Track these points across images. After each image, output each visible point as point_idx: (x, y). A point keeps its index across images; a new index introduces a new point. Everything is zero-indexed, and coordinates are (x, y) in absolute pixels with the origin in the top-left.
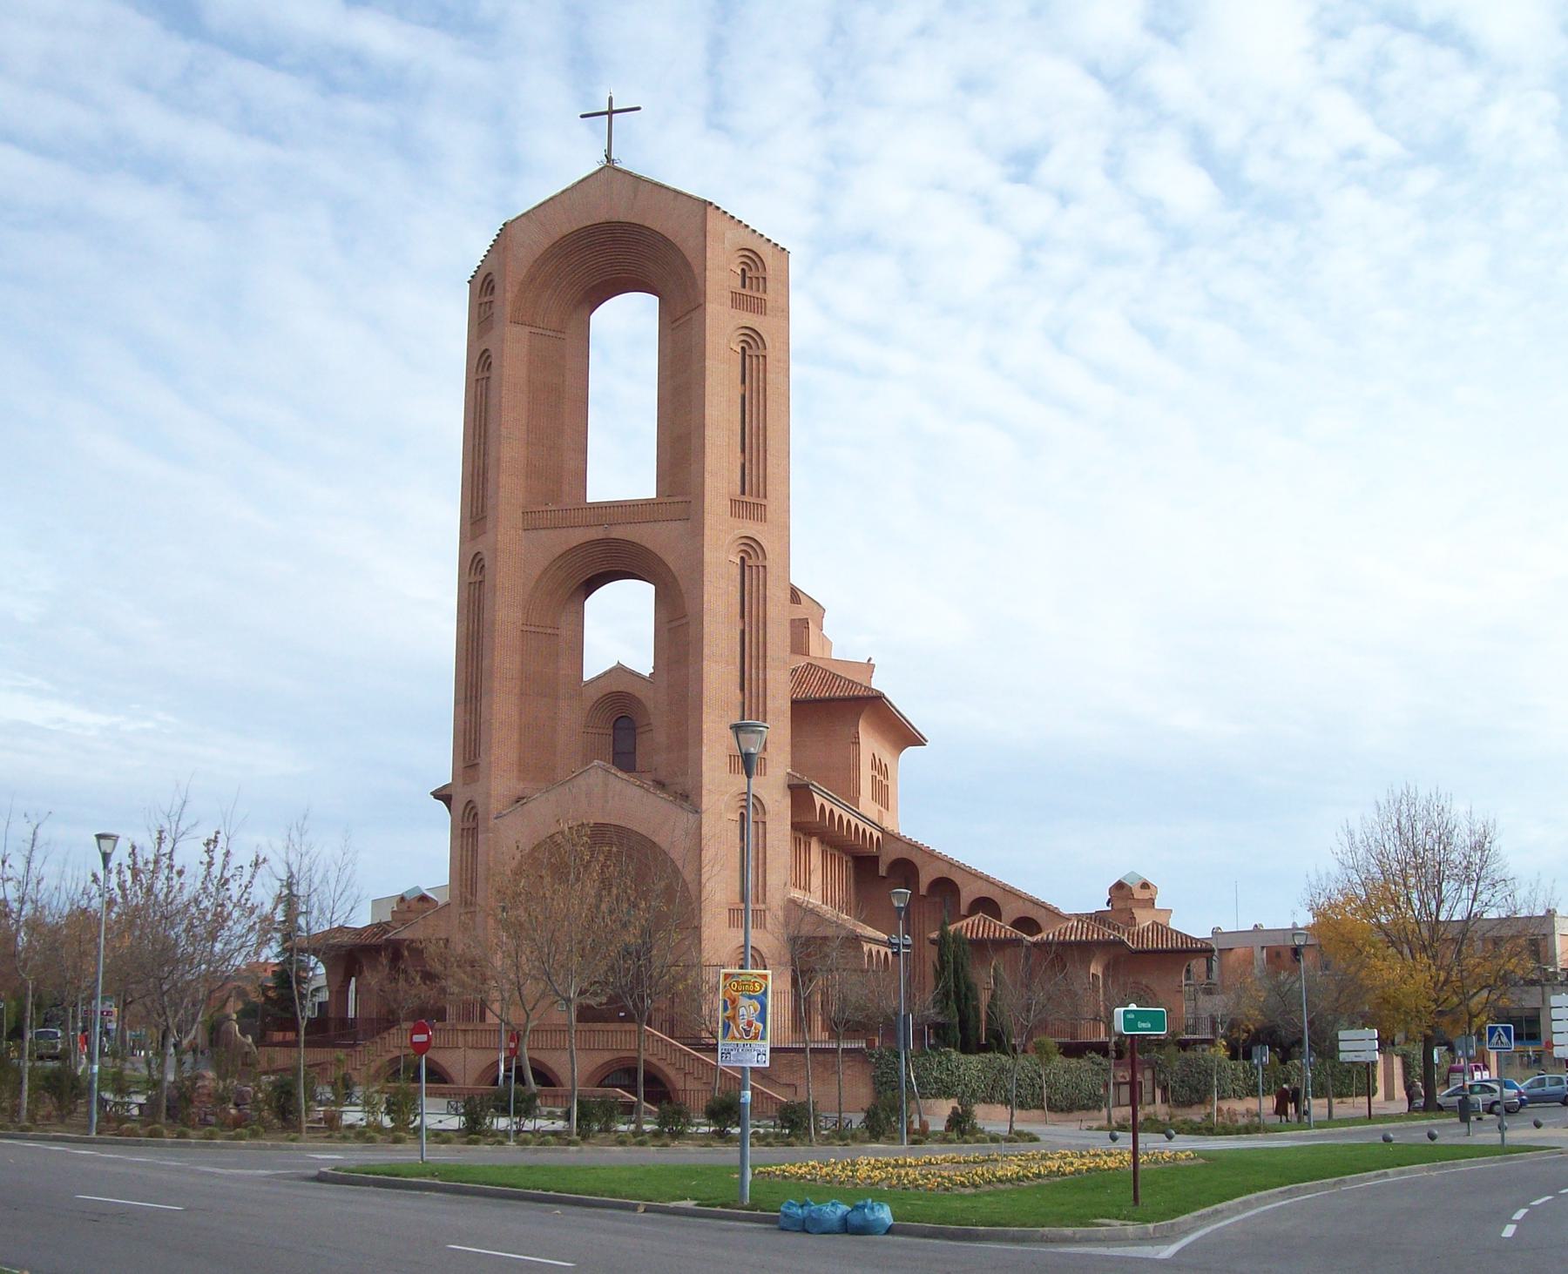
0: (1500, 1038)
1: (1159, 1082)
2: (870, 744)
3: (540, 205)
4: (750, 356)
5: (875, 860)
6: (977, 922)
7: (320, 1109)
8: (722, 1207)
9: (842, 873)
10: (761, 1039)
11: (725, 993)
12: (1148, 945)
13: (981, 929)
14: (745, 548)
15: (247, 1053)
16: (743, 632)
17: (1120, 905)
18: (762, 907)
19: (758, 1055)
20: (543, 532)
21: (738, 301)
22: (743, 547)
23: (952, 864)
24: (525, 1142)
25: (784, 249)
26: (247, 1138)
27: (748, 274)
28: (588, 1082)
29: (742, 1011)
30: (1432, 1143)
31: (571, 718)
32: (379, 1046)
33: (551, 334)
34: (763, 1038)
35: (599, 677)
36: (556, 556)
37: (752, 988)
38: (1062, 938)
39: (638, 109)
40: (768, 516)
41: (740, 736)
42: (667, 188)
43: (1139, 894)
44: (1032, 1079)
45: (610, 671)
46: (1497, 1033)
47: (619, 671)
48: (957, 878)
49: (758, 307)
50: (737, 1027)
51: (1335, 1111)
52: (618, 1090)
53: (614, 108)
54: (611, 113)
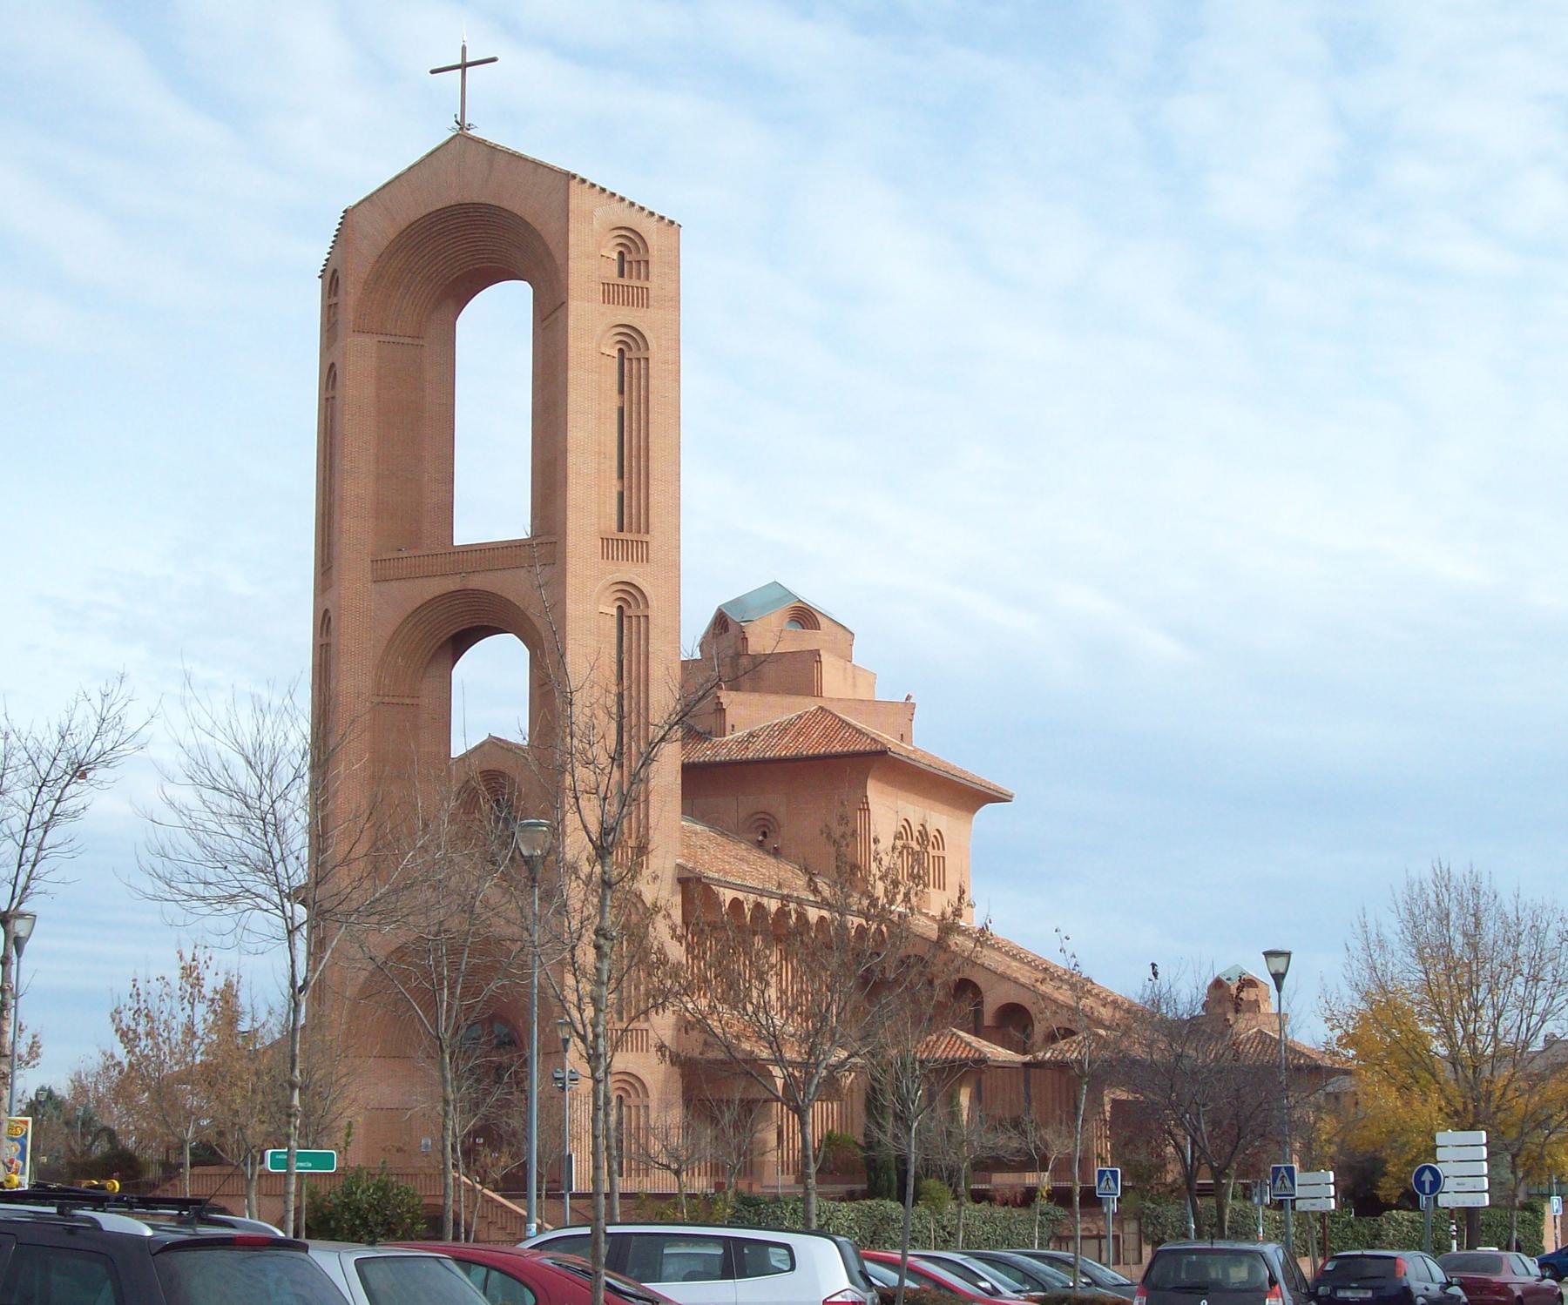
1: (1147, 1237)
14: (623, 596)
21: (611, 294)
22: (619, 595)
25: (672, 223)
27: (628, 258)
33: (408, 340)
34: (23, 1173)
36: (410, 611)
39: (494, 60)
40: (651, 555)
47: (494, 745)
49: (640, 298)
53: (468, 60)
54: (464, 66)
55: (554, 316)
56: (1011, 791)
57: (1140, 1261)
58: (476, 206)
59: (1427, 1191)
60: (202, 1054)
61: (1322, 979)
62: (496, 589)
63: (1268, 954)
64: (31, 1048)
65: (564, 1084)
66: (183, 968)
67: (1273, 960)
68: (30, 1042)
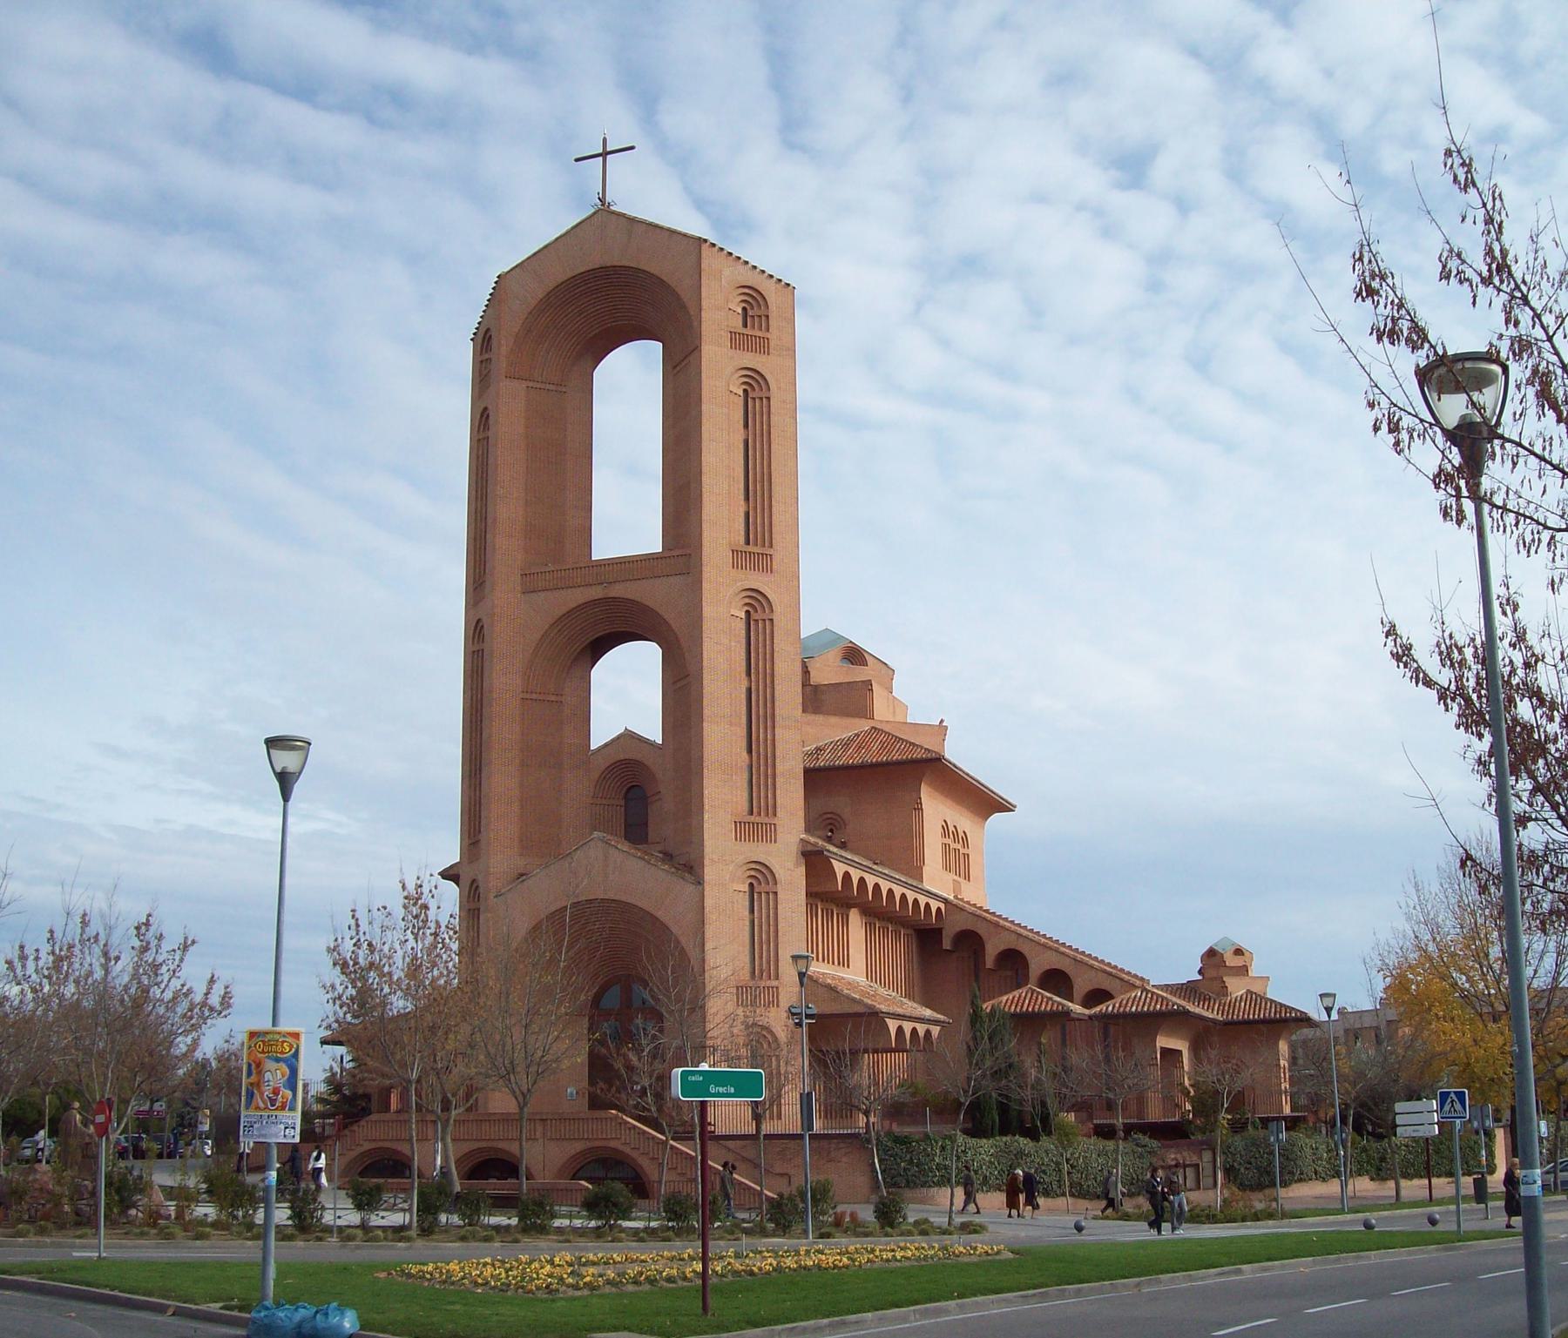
2: (936, 810)
3: (535, 254)
4: (754, 399)
5: (936, 933)
6: (1024, 994)
7: (168, 1203)
8: (239, 1311)
9: (897, 952)
10: (289, 1110)
11: (249, 1054)
12: (1238, 1016)
13: (1027, 1001)
15: (87, 1144)
16: (749, 690)
17: (1211, 973)
18: (775, 983)
19: (286, 1128)
21: (739, 341)
22: (747, 600)
23: (1018, 932)
24: (350, 1238)
25: (788, 285)
26: (31, 1235)
27: (750, 313)
28: (560, 1175)
29: (268, 1076)
30: (1433, 1229)
31: (577, 790)
32: (348, 1139)
33: (551, 387)
34: (292, 1109)
35: (606, 745)
37: (279, 1048)
38: (1122, 1009)
39: (632, 148)
40: (774, 567)
41: (271, 751)
42: (661, 228)
43: (1231, 961)
44: (1058, 1164)
45: (618, 738)
47: (629, 738)
48: (1025, 949)
49: (762, 346)
50: (262, 1094)
51: (1403, 1193)
52: (583, 1182)
54: (605, 154)
58: (616, 269)
61: (1374, 934)
64: (223, 998)
65: (801, 1019)
66: (406, 898)
68: (222, 993)
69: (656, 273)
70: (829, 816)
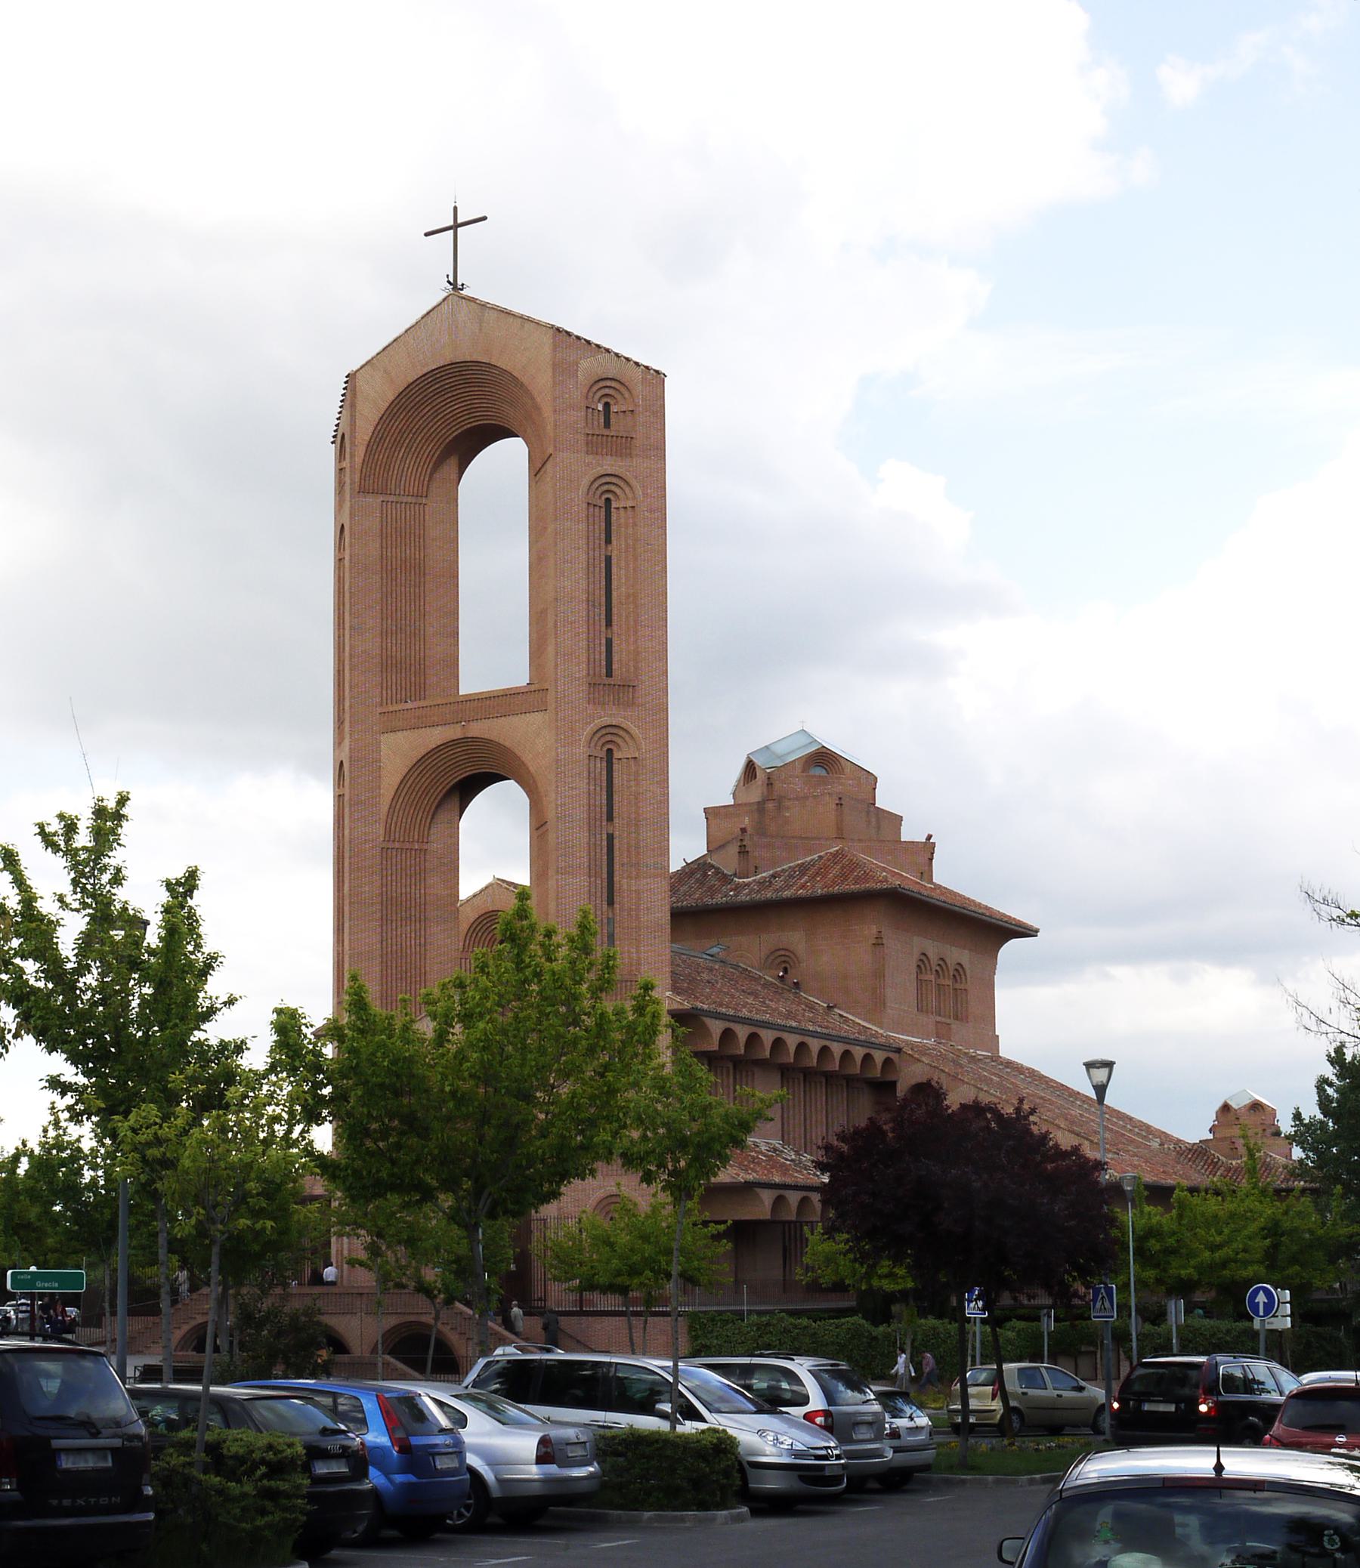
0: (1103, 1303)
20: (399, 734)
33: (409, 499)
46: (1100, 1296)
53: (459, 221)
54: (455, 227)
55: (543, 470)
56: (1036, 926)
57: (1119, 1378)
59: (1261, 1314)
60: (228, 1174)
62: (493, 736)
63: (1090, 1066)
67: (1093, 1071)
69: (508, 368)
70: (783, 953)
